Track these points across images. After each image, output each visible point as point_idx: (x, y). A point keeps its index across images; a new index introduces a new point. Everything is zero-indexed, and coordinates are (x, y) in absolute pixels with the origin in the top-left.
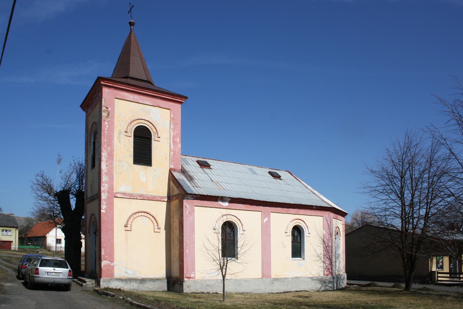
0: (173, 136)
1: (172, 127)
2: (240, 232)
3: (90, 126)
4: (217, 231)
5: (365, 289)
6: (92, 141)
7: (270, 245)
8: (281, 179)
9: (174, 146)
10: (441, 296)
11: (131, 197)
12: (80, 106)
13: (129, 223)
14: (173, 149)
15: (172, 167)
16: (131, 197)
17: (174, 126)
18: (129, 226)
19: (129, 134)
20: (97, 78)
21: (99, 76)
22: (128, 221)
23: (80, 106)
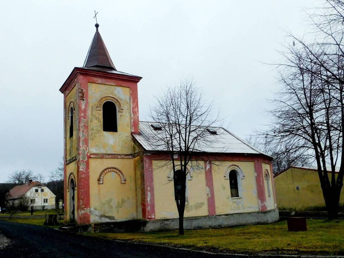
0: (133, 107)
1: (132, 101)
2: (206, 185)
3: (68, 104)
4: (170, 179)
5: (127, 157)
6: (70, 115)
7: (213, 186)
8: (217, 134)
9: (134, 115)
10: (280, 224)
11: (102, 156)
12: (59, 90)
13: (102, 177)
14: (133, 117)
15: (133, 131)
16: (102, 156)
17: (133, 100)
18: (101, 180)
19: (226, 178)
20: (74, 68)
21: (75, 67)
22: (100, 176)
23: (59, 90)
